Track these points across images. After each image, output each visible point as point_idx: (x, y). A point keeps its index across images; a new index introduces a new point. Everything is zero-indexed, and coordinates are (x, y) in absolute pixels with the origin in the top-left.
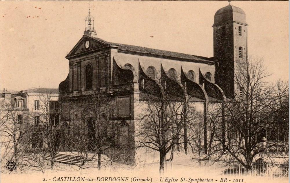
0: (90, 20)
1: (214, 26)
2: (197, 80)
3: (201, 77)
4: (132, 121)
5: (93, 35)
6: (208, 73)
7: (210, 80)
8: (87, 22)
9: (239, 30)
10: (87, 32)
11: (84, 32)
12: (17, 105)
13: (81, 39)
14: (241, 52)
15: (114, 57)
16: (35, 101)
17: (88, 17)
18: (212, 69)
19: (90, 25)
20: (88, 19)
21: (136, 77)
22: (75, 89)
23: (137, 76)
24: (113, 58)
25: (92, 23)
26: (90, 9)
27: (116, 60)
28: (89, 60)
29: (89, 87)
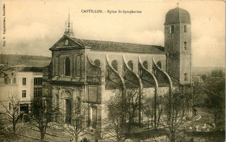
0: (69, 24)
1: (165, 24)
2: (150, 70)
3: (154, 68)
4: (100, 105)
5: (71, 36)
6: (159, 64)
7: (161, 68)
8: (67, 25)
9: (185, 28)
10: (68, 32)
11: (65, 32)
12: (9, 82)
13: (62, 38)
14: (186, 45)
15: (87, 55)
16: (23, 78)
17: (68, 21)
18: (162, 57)
19: (69, 27)
20: (68, 23)
21: (103, 73)
22: (56, 74)
23: (104, 72)
24: (87, 56)
25: (71, 25)
26: (69, 15)
27: (88, 57)
28: (68, 55)
29: (68, 73)
